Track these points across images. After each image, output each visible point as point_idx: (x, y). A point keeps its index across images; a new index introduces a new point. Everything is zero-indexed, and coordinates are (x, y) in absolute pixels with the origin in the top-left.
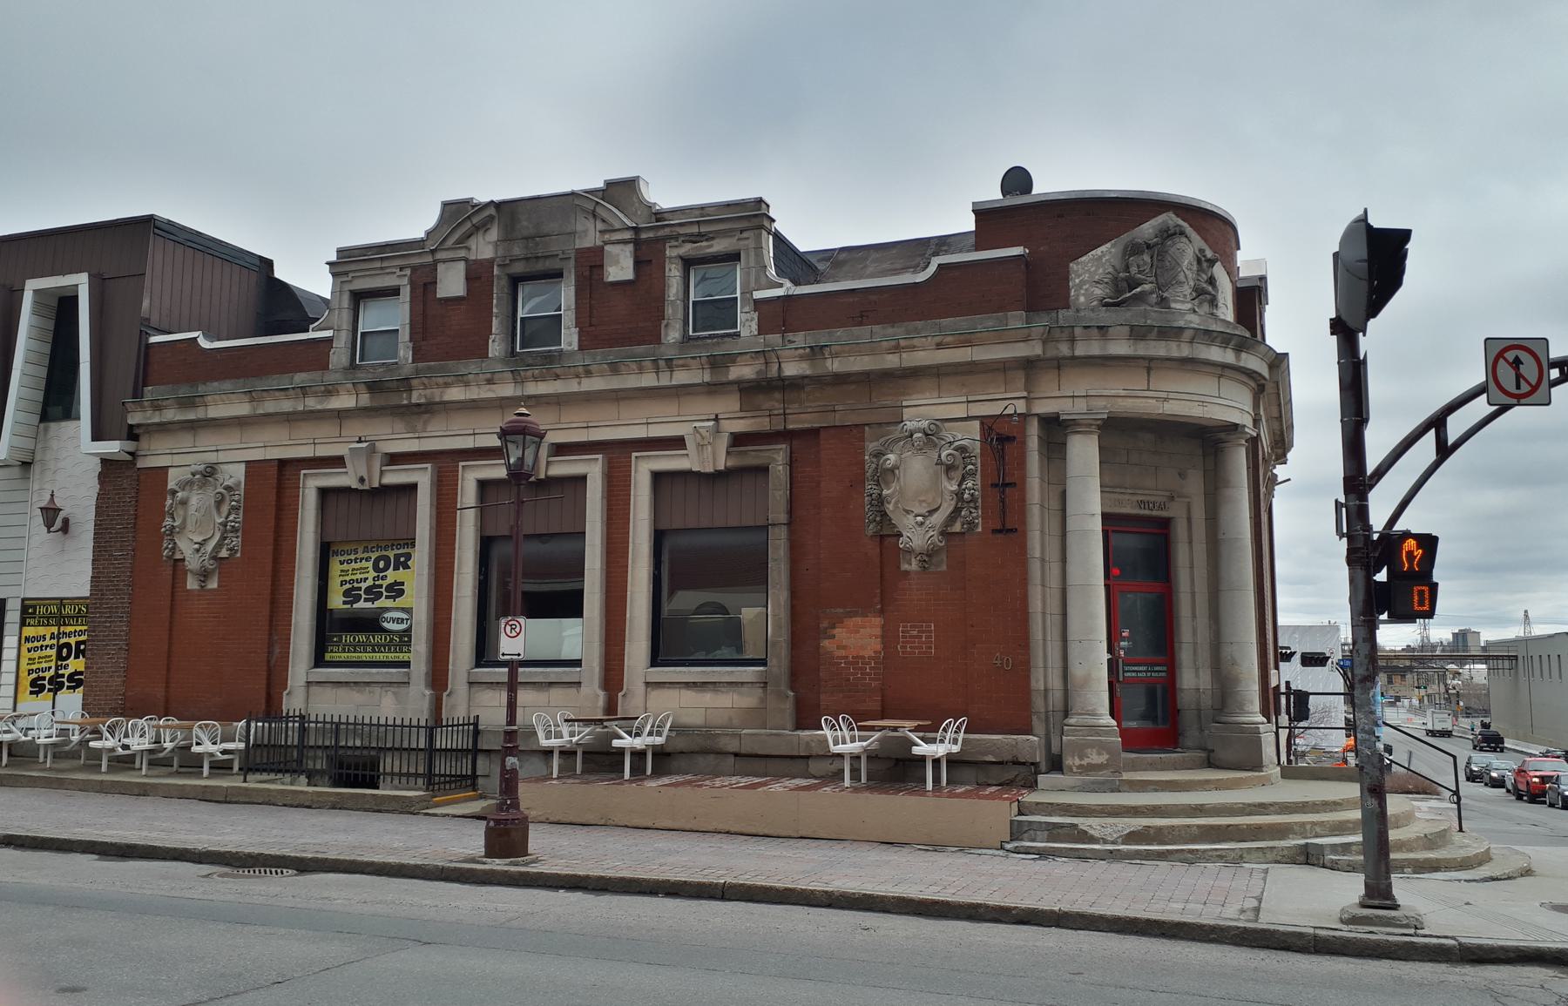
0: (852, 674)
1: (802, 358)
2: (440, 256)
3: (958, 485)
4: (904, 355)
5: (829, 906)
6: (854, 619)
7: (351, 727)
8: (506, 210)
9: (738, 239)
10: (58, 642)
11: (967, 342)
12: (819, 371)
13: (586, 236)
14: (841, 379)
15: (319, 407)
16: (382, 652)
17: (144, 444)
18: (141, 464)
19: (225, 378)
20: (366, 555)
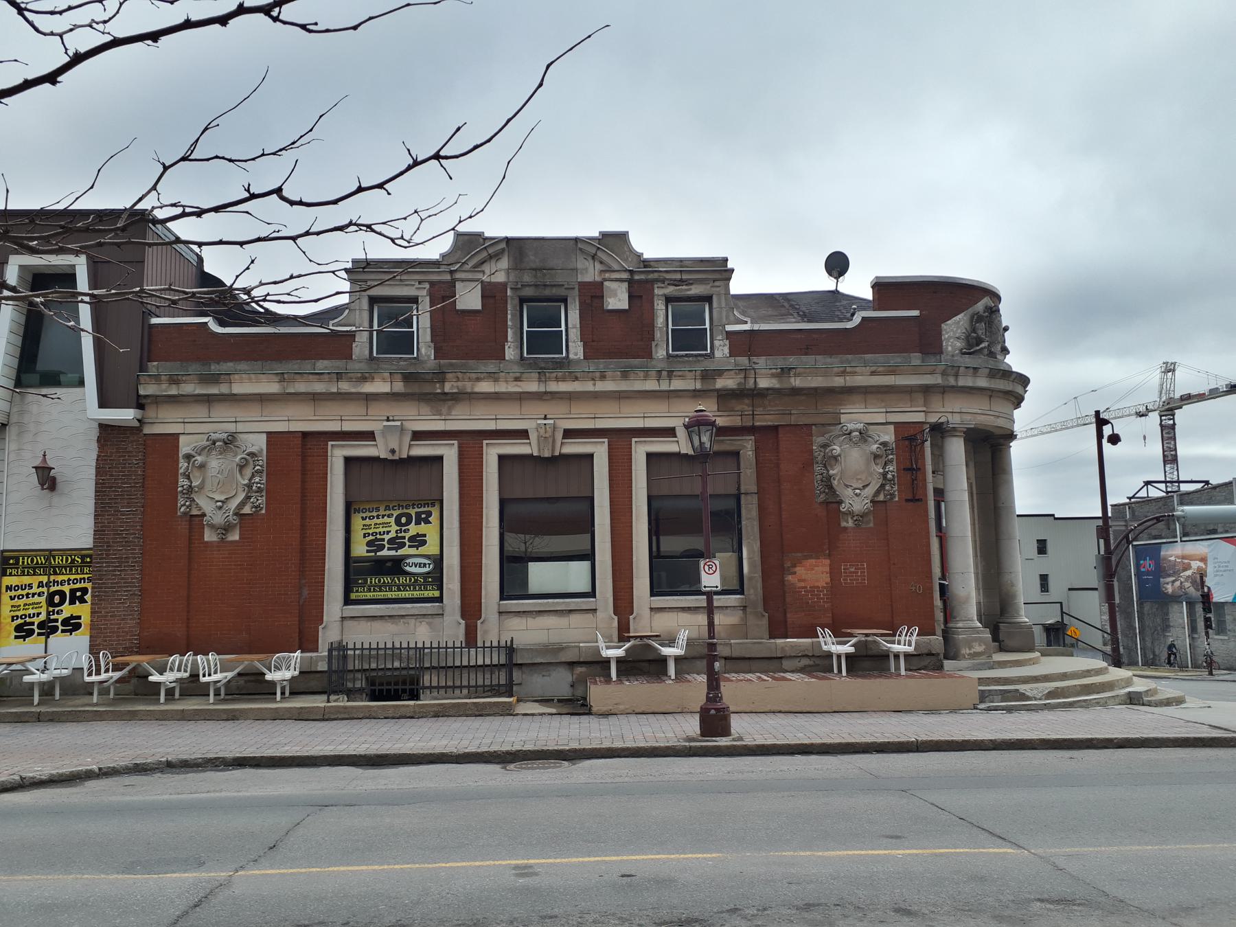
0: (811, 599)
1: (773, 376)
2: (458, 276)
3: (249, 480)
4: (847, 378)
5: (994, 749)
6: (809, 560)
7: (388, 652)
8: (515, 246)
9: (712, 287)
10: (48, 590)
11: (892, 371)
12: (786, 386)
13: (587, 272)
14: (796, 392)
15: (353, 390)
16: (407, 591)
17: (151, 413)
18: (147, 430)
19: (241, 360)
20: (387, 512)
